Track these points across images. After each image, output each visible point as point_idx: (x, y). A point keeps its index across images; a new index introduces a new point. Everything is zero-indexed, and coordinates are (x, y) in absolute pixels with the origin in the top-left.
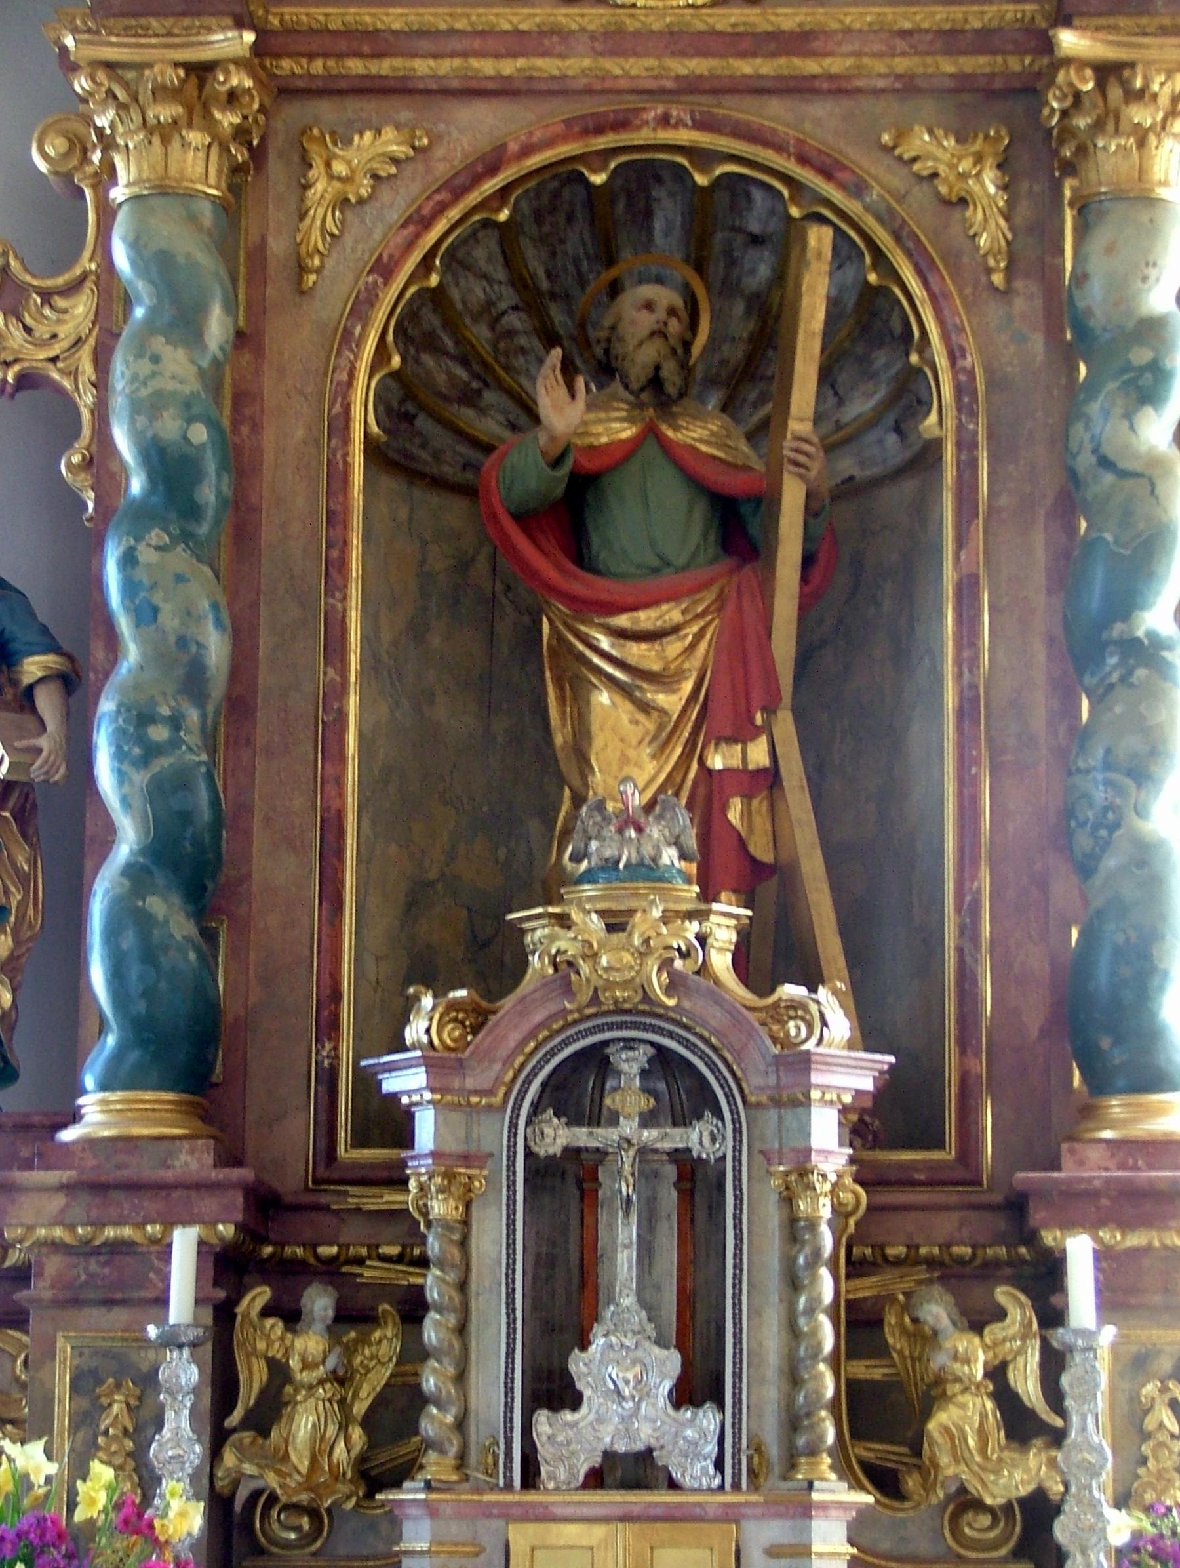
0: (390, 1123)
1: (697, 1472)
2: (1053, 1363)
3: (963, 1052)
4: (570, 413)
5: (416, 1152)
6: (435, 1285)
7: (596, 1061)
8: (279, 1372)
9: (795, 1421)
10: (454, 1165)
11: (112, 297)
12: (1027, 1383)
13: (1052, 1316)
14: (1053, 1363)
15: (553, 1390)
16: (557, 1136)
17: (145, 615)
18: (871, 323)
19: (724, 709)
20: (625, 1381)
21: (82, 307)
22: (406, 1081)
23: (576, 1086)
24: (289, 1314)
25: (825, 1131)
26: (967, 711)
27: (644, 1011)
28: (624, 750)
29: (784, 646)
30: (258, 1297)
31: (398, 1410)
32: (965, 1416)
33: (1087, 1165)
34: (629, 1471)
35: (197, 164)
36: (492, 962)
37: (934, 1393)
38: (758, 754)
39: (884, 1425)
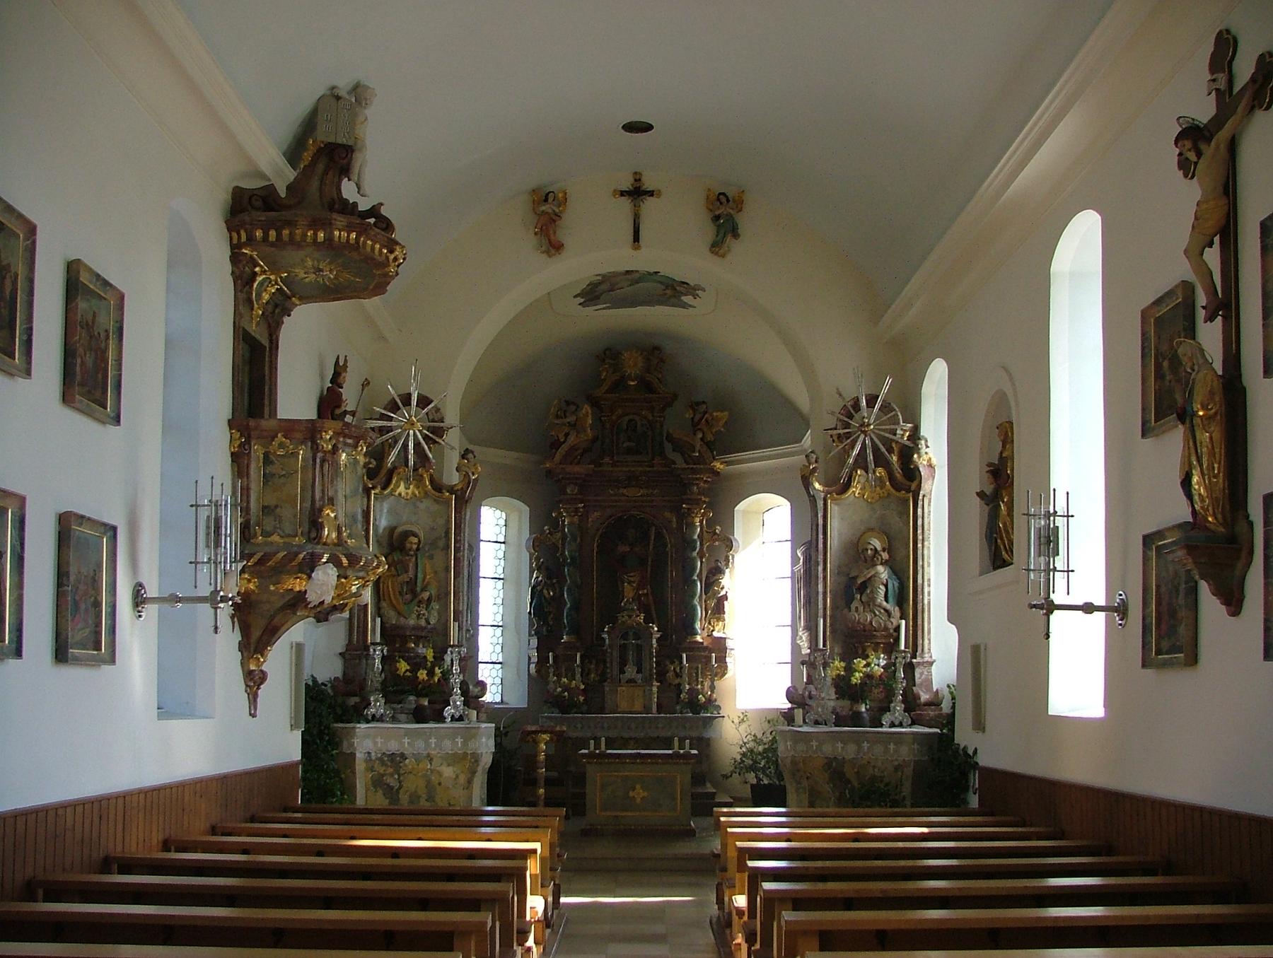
0: (604, 639)
3: (218, 521)
5: (1191, 276)
7: (627, 633)
9: (651, 675)
18: (659, 535)
19: (641, 585)
20: (631, 671)
22: (605, 636)
28: (629, 591)
31: (603, 674)
32: (671, 674)
34: (630, 681)
35: (576, 519)
39: (661, 676)
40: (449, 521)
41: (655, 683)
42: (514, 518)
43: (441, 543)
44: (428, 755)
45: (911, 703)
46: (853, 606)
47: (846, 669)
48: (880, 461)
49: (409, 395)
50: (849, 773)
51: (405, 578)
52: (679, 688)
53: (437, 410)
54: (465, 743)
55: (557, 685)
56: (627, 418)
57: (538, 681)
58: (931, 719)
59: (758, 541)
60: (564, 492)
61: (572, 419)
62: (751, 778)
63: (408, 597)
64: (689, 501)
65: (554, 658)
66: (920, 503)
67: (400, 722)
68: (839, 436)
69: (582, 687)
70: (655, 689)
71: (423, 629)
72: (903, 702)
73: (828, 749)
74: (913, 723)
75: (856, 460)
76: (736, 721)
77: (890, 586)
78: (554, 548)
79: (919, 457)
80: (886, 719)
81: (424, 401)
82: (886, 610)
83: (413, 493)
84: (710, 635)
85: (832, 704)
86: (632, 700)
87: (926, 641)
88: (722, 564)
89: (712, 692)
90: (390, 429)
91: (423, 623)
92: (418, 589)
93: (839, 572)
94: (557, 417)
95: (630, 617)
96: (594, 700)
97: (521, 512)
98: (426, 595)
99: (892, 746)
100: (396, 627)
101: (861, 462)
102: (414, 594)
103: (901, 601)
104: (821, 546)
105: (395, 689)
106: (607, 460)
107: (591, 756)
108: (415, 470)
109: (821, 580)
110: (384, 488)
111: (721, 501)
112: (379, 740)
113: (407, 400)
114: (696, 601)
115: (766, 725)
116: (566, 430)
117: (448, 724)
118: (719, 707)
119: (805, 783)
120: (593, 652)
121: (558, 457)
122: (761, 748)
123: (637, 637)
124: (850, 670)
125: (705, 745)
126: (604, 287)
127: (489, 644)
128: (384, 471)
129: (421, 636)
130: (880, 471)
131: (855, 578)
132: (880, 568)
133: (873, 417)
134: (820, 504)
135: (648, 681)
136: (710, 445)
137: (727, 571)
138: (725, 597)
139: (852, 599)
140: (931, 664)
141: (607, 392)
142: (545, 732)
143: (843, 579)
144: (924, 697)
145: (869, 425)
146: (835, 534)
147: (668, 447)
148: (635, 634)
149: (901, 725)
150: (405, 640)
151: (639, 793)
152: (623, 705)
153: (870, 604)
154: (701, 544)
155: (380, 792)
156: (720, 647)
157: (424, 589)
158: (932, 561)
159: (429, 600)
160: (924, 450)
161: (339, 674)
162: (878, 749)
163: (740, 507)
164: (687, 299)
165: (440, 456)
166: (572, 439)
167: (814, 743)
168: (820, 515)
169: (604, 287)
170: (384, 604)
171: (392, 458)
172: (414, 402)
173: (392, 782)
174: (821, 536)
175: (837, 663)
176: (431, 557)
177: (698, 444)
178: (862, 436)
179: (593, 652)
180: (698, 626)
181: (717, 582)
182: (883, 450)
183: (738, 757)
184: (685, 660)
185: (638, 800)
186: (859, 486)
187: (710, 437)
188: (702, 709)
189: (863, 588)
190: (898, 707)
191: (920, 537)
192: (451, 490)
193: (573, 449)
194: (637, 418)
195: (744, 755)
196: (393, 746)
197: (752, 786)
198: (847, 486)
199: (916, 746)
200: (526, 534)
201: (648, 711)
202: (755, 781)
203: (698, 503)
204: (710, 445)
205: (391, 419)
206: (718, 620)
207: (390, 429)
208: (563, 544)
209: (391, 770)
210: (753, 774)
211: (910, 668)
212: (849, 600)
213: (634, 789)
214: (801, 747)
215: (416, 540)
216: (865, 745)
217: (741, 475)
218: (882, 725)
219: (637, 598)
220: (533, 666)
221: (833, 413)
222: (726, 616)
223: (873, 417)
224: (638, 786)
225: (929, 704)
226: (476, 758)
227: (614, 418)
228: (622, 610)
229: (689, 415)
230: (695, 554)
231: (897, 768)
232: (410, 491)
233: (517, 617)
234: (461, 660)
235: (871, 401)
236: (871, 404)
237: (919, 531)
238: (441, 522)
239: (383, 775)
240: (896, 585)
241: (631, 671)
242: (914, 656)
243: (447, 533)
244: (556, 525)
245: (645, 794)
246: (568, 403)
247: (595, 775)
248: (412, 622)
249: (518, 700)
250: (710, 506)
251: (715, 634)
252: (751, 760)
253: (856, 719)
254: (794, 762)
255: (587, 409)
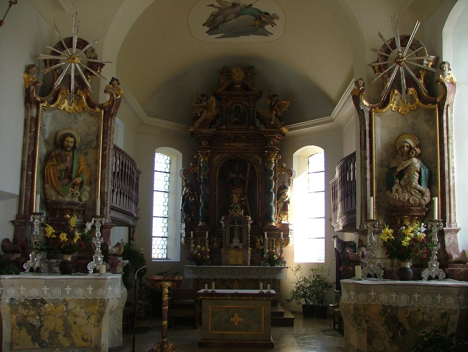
0: (221, 224)
1: (241, 247)
2: (264, 240)
4: (232, 175)
6: (224, 235)
7: (234, 221)
8: (213, 241)
9: (247, 244)
10: (225, 228)
11: (200, 168)
12: (262, 241)
13: (264, 237)
14: (264, 240)
15: (231, 242)
16: (232, 226)
17: (204, 190)
18: (252, 168)
19: (242, 196)
20: (236, 242)
21: (198, 168)
22: (222, 222)
23: (233, 223)
24: (214, 237)
25: (249, 225)
26: (259, 196)
27: (237, 217)
28: (236, 199)
29: (246, 191)
30: (212, 236)
31: (221, 243)
32: (258, 244)
33: (266, 228)
34: (236, 247)
35: (207, 159)
36: (227, 214)
37: (256, 242)
38: (245, 199)
39: (253, 244)
40: (98, 129)
41: (249, 249)
42: (175, 159)
43: (93, 145)
44: (64, 300)
45: (445, 260)
46: (394, 189)
47: (394, 234)
48: (411, 83)
49: (71, 39)
50: (402, 318)
51: (62, 166)
52: (262, 251)
53: (93, 51)
54: (94, 291)
55: (196, 249)
56: (235, 106)
57: (185, 247)
58: (461, 274)
59: (305, 173)
60: (200, 144)
61: (204, 104)
62: (303, 301)
63: (66, 181)
64: (269, 149)
65: (194, 234)
66: (445, 111)
67: (55, 273)
68: (380, 66)
69: (209, 250)
70: (249, 252)
71: (77, 204)
72: (438, 260)
73: (384, 298)
74: (447, 277)
75: (392, 85)
76: (294, 270)
77: (423, 173)
78: (195, 175)
79: (444, 76)
80: (425, 273)
81: (82, 44)
82: (420, 191)
83: (74, 109)
84: (280, 223)
85: (379, 261)
86: (237, 258)
87: (452, 214)
88: (286, 184)
89: (281, 254)
90: (57, 61)
91: (76, 200)
92: (73, 175)
93: (381, 165)
94: (197, 103)
95: (236, 212)
96: (216, 257)
97: (178, 156)
98: (79, 180)
99: (439, 297)
100: (57, 203)
101: (397, 84)
102: (70, 178)
103: (431, 183)
104: (368, 146)
105: (52, 248)
106: (224, 127)
107: (206, 294)
108: (75, 92)
109: (368, 171)
110: (53, 102)
111: (286, 149)
112: (22, 288)
113: (69, 42)
114: (272, 204)
115: (311, 272)
116: (201, 110)
117: (91, 275)
118: (285, 262)
119: (364, 324)
120: (215, 231)
121: (197, 125)
122: (308, 285)
123: (240, 223)
124: (399, 235)
125: (276, 284)
126: (220, 18)
127: (159, 227)
128: (53, 92)
129: (71, 208)
130: (411, 90)
131: (395, 168)
132: (415, 160)
133: (405, 53)
134: (367, 116)
135: (245, 248)
136: (280, 118)
137: (289, 187)
138: (288, 202)
139: (393, 184)
140: (457, 231)
141: (224, 90)
142: (166, 281)
143: (385, 170)
144: (455, 257)
145: (402, 58)
146: (378, 138)
147: (257, 121)
148: (238, 221)
149: (437, 278)
150: (63, 212)
151: (237, 319)
152: (232, 261)
153: (407, 187)
154: (275, 173)
155: (24, 330)
156: (285, 229)
157: (78, 176)
158: (455, 154)
159: (82, 183)
160: (447, 72)
161: (11, 237)
162: (427, 300)
163: (296, 154)
164: (268, 28)
165: (97, 85)
166: (204, 116)
167: (373, 293)
168: (367, 123)
169: (220, 18)
170: (47, 186)
171: (58, 82)
172: (75, 45)
173: (35, 321)
174: (368, 139)
175: (388, 231)
176: (86, 154)
177: (274, 117)
178: (398, 66)
179: (215, 231)
180: (273, 217)
181: (284, 193)
182: (413, 75)
183: (295, 290)
184: (268, 236)
185: (236, 324)
186: (395, 102)
187: (280, 114)
188: (276, 263)
189: (401, 175)
190: (435, 265)
191: (445, 136)
192: (101, 107)
193: (205, 120)
194: (240, 105)
195: (298, 288)
196: (34, 293)
197: (303, 305)
198: (386, 103)
199: (461, 297)
200: (180, 167)
201: (245, 264)
202: (304, 303)
203: (273, 150)
204: (280, 118)
205: (59, 55)
206: (284, 214)
207: (57, 61)
208: (200, 173)
209: (32, 312)
210: (303, 299)
211: (441, 234)
212: (389, 186)
213: (233, 316)
214: (362, 296)
215: (71, 140)
216: (416, 295)
217: (297, 136)
218: (421, 279)
219: (240, 202)
220: (183, 239)
221: (374, 50)
222: (289, 212)
223: (405, 53)
224: (236, 315)
225: (458, 262)
226: (103, 303)
227: (228, 105)
228: (231, 208)
229: (268, 102)
230: (272, 178)
231: (443, 315)
232: (72, 107)
233: (175, 214)
234: (102, 228)
235: (404, 40)
236: (403, 45)
237: (445, 132)
238: (94, 129)
239: (26, 317)
240: (427, 172)
241: (236, 242)
242: (445, 226)
243: (98, 138)
244: (196, 162)
245: (241, 320)
246: (203, 96)
247: (208, 307)
248: (68, 199)
249: (175, 257)
250: (279, 153)
251: (283, 222)
252: (301, 292)
253: (403, 274)
254: (356, 308)
255: (213, 99)
